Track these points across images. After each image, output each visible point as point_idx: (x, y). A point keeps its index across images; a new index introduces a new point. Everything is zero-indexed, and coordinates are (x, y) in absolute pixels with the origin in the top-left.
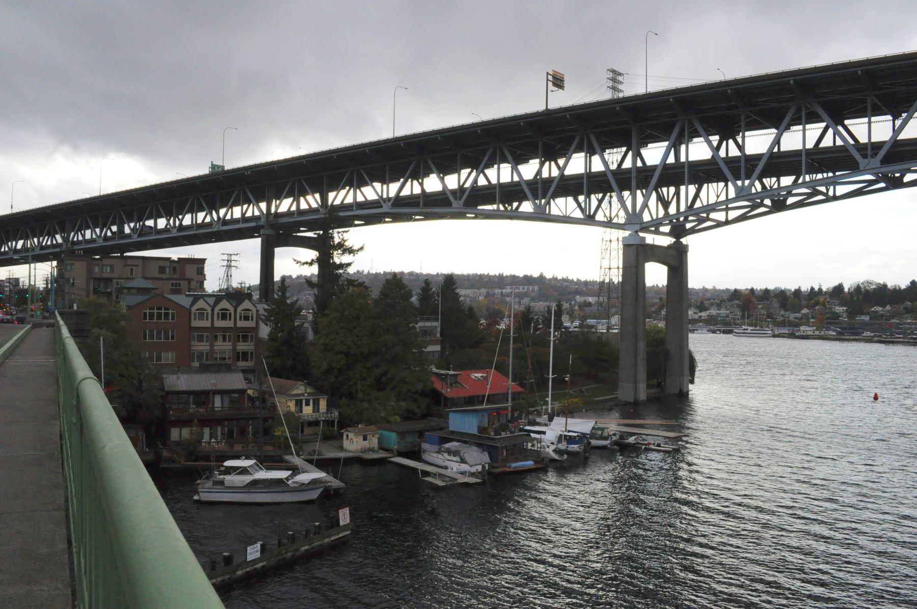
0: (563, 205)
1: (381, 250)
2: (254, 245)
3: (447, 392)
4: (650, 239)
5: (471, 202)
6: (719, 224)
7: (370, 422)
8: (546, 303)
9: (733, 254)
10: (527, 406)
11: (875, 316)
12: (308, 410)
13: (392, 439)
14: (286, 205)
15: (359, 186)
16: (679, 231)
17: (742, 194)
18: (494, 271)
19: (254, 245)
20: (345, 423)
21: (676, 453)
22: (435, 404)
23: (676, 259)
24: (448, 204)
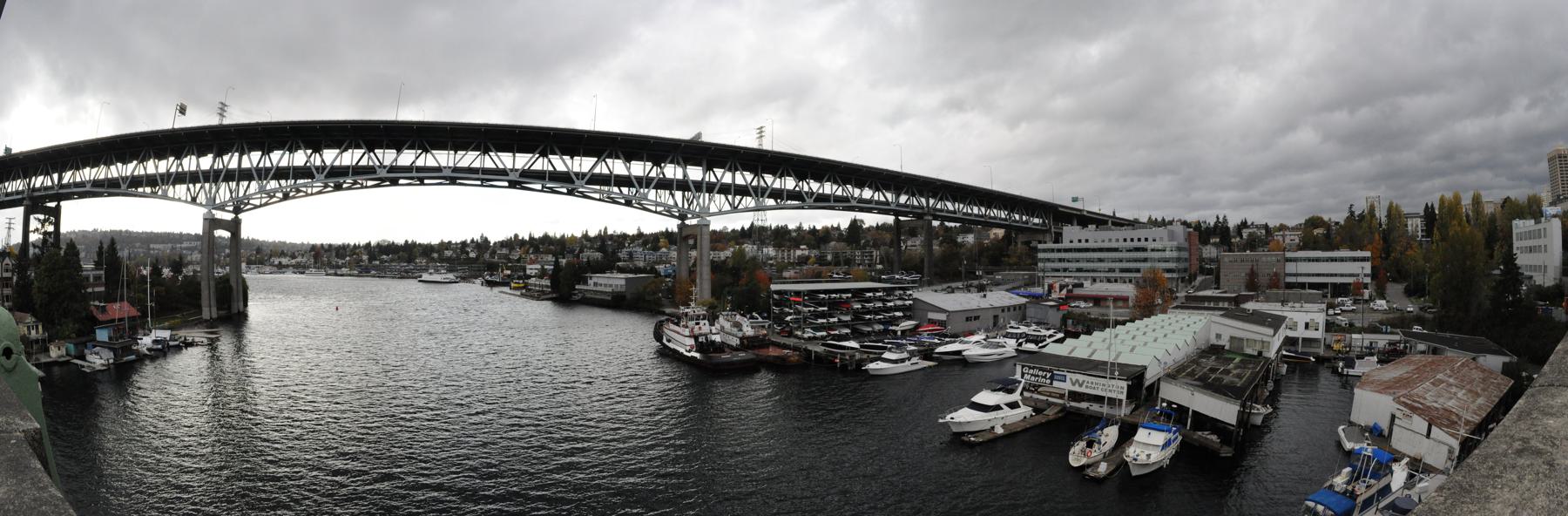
0: (181, 190)
1: (83, 217)
2: (19, 212)
3: (101, 317)
4: (219, 215)
5: (132, 185)
6: (256, 207)
7: (60, 339)
8: (167, 252)
9: (268, 223)
10: (137, 325)
11: (382, 262)
12: (33, 332)
13: (72, 347)
14: (38, 181)
15: (78, 169)
16: (237, 210)
17: (262, 190)
18: (177, 230)
19: (19, 212)
20: (51, 340)
21: (239, 349)
22: (92, 323)
23: (234, 227)
24: (119, 186)
